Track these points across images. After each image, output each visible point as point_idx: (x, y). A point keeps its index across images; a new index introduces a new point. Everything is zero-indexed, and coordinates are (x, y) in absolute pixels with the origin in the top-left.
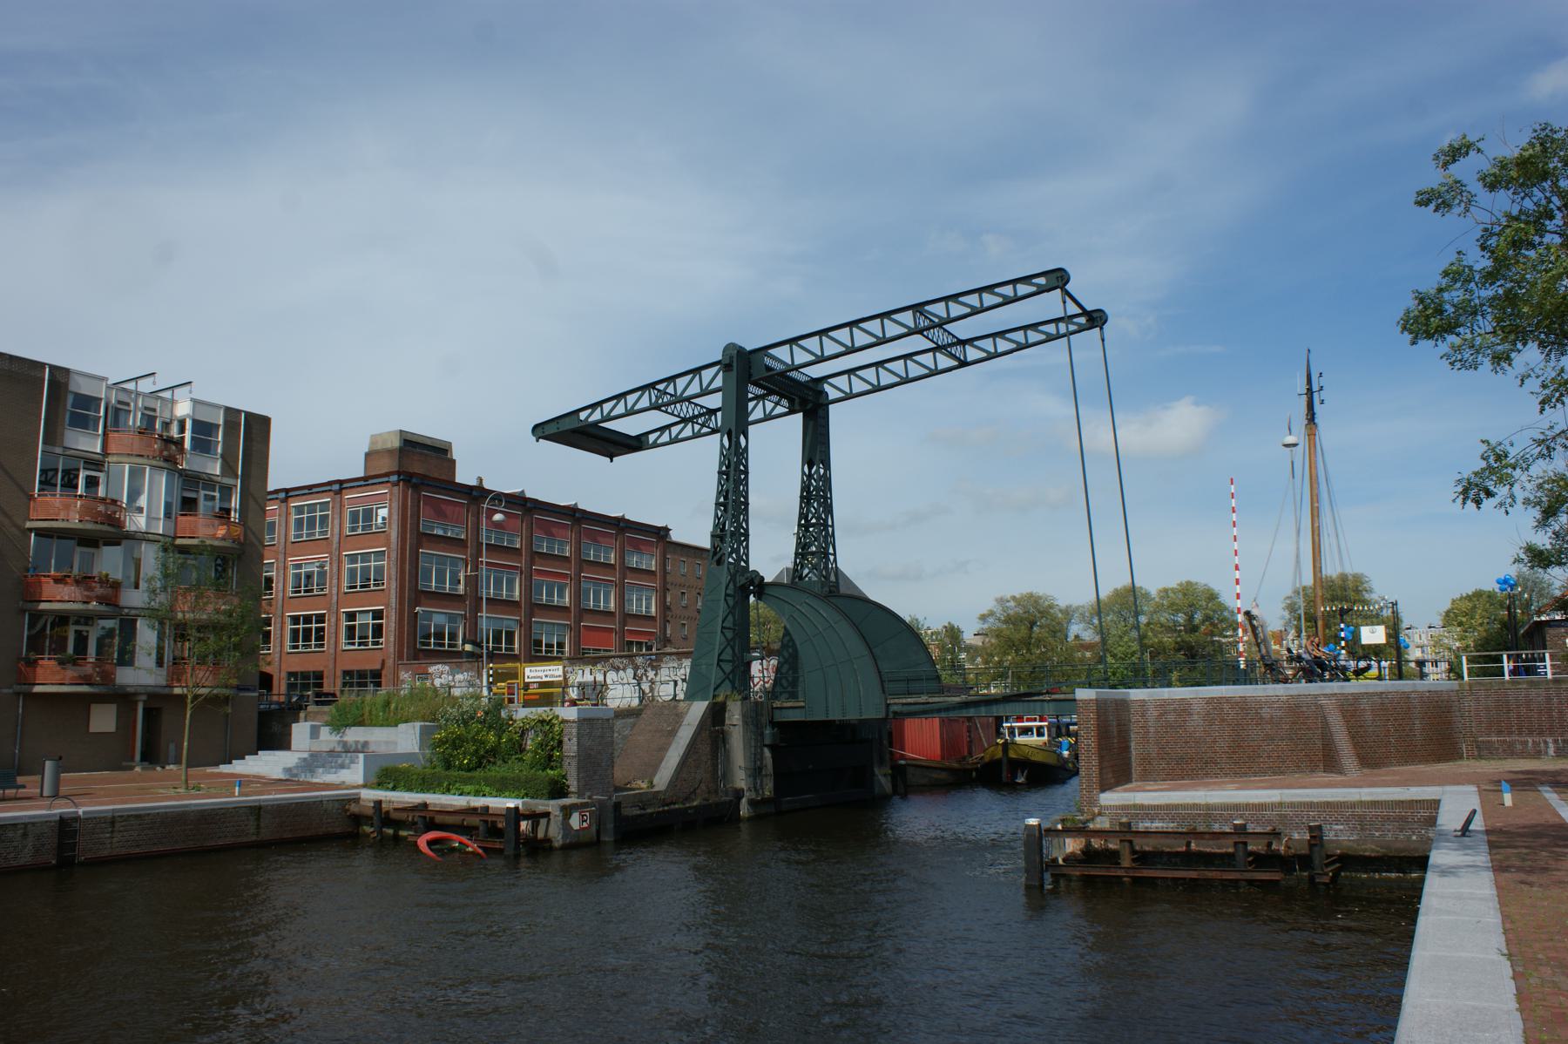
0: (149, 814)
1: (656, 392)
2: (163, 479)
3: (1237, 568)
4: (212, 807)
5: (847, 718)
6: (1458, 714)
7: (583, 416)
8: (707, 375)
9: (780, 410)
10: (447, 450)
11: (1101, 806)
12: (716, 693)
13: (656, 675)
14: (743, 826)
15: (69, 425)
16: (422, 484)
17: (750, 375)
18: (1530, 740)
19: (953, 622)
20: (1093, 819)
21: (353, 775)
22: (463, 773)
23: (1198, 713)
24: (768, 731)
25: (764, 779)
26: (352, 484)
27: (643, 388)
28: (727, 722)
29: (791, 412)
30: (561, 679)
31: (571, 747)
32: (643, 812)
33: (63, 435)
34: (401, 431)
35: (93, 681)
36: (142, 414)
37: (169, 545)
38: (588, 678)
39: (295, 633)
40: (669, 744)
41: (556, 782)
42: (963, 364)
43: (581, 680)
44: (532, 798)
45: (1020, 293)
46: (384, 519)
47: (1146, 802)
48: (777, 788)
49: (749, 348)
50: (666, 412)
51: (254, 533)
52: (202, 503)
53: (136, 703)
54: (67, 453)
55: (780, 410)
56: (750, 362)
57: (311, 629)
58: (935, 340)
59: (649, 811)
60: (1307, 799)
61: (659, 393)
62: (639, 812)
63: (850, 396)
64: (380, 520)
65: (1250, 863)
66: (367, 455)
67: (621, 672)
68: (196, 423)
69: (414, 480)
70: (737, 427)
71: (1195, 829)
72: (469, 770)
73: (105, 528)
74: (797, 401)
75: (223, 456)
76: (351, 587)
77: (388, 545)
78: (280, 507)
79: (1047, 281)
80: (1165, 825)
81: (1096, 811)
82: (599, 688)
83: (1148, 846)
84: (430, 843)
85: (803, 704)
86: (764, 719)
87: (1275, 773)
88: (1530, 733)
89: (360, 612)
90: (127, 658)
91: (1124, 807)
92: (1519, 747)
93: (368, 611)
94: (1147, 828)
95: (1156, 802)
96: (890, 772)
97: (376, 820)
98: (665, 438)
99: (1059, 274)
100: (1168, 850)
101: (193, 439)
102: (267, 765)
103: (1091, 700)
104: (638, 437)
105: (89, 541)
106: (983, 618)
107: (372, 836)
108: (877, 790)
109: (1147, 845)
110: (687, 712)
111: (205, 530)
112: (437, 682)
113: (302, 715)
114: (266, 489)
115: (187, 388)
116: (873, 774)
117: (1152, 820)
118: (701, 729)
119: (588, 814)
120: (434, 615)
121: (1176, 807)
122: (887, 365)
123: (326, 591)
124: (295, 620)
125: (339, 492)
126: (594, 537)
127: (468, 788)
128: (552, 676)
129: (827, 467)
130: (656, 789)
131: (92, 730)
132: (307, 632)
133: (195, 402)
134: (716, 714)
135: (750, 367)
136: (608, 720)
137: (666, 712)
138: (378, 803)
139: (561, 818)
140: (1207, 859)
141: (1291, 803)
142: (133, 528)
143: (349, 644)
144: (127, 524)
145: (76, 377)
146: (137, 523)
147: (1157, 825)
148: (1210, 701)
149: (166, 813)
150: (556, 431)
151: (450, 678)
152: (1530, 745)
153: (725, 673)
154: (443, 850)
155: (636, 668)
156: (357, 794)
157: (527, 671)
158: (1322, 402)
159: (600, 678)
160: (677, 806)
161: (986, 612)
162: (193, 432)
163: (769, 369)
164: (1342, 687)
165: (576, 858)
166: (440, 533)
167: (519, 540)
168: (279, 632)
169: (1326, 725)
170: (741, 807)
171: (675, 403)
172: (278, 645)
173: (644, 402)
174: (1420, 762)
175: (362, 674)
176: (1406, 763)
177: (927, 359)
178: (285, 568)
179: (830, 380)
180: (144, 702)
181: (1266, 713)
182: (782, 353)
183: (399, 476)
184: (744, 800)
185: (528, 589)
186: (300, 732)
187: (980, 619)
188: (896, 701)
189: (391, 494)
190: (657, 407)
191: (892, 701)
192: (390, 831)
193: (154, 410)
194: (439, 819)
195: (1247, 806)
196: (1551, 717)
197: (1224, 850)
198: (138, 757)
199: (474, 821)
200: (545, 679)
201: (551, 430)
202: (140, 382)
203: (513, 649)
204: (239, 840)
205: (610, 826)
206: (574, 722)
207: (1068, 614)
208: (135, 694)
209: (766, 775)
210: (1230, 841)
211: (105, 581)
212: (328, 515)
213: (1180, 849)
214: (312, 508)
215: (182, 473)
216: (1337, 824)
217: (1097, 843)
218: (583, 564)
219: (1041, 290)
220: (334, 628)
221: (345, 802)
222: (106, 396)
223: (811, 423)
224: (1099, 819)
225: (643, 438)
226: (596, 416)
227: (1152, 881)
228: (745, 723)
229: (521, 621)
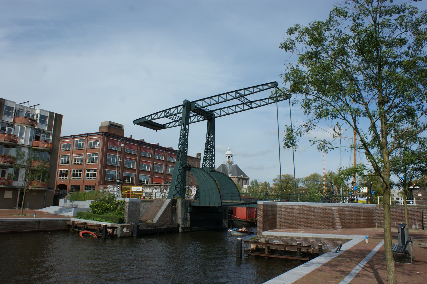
0: (5, 221)
1: (166, 112)
2: (30, 130)
3: (324, 169)
4: (25, 220)
5: (215, 206)
6: (375, 214)
7: (147, 118)
8: (180, 108)
9: (201, 119)
10: (122, 127)
11: (262, 235)
12: (174, 197)
13: (166, 191)
14: (180, 234)
15: (4, 114)
16: (109, 135)
17: (191, 109)
18: (396, 223)
19: (266, 181)
20: (260, 239)
21: (70, 214)
22: (98, 215)
23: (296, 210)
24: (189, 208)
25: (187, 222)
26: (91, 135)
27: (162, 111)
28: (177, 205)
29: (204, 120)
30: (141, 191)
31: (127, 209)
32: (147, 229)
33: (2, 117)
34: (109, 121)
35: (5, 184)
36: (26, 112)
37: (30, 148)
38: (148, 191)
39: (74, 174)
40: (159, 210)
41: (121, 219)
42: (251, 108)
43: (146, 191)
44: (114, 223)
45: (264, 88)
46: (98, 144)
47: (275, 235)
48: (191, 224)
49: (191, 101)
50: (169, 118)
51: (56, 146)
52: (41, 137)
53: (18, 191)
54: (3, 122)
55: (201, 119)
56: (191, 105)
57: (78, 174)
58: (242, 101)
59: (149, 228)
60: (320, 237)
61: (167, 113)
62: (145, 229)
63: (220, 116)
64: (97, 145)
65: (301, 255)
66: (100, 127)
67: (157, 190)
68: (41, 116)
69: (107, 134)
70: (186, 122)
71: (288, 244)
72: (100, 214)
73: (12, 143)
74: (206, 116)
75: (48, 125)
76: (89, 163)
77: (99, 152)
78: (72, 140)
79: (272, 85)
80: (280, 242)
81: (261, 237)
82: (151, 194)
83: (274, 248)
84: (83, 234)
85: (199, 201)
86: (188, 205)
87: (318, 229)
88: (396, 221)
89: (91, 170)
90: (16, 179)
91: (269, 236)
92: (392, 225)
93: (93, 170)
94: (275, 243)
95: (278, 235)
96: (228, 222)
97: (72, 226)
98: (171, 125)
99: (275, 83)
100: (279, 249)
101: (40, 120)
102: (51, 210)
103: (262, 204)
104: (164, 125)
105: (8, 146)
106: (274, 180)
107: (71, 231)
108: (223, 226)
109: (273, 248)
110: (165, 202)
111: (41, 145)
112: (109, 190)
113: (66, 197)
114: (60, 135)
115: (38, 106)
116: (222, 222)
117: (276, 240)
118: (168, 206)
119: (129, 228)
120: (111, 171)
121: (283, 237)
122: (231, 108)
123: (82, 164)
124: (74, 171)
125: (87, 137)
126: (158, 153)
127: (98, 219)
128: (139, 190)
129: (214, 135)
130: (153, 222)
131: (5, 197)
132: (77, 174)
133: (41, 110)
134: (174, 202)
135: (191, 107)
136: (139, 202)
137: (160, 201)
138: (74, 222)
139: (120, 229)
140: (291, 253)
141: (316, 238)
142: (20, 143)
143: (87, 178)
144: (19, 142)
145: (7, 102)
146: (22, 142)
147: (277, 242)
148: (300, 206)
149: (11, 221)
150: (139, 122)
151: (113, 189)
152: (396, 224)
153: (177, 191)
154: (86, 236)
155: (161, 189)
156: (70, 219)
157: (133, 188)
158: (358, 123)
159: (151, 191)
160: (158, 228)
161: (275, 179)
162: (40, 118)
163: (196, 107)
164: (316, 204)
165: (125, 241)
166: (114, 149)
167: (137, 152)
168: (69, 174)
169: (333, 215)
170: (179, 229)
171: (172, 116)
172: (69, 177)
173: (163, 115)
174: (362, 228)
175: (90, 187)
176: (358, 228)
177: (241, 106)
178: (72, 157)
179: (215, 111)
180: (20, 191)
181: (316, 211)
182: (200, 103)
183: (103, 133)
184: (180, 227)
185: (138, 166)
186: (61, 201)
187: (273, 181)
188: (224, 202)
189: (101, 138)
190: (166, 117)
191: (223, 202)
192: (77, 230)
193: (30, 112)
194: (89, 227)
195: (303, 238)
196: (402, 216)
197: (295, 251)
198: (17, 206)
199: (97, 228)
200: (137, 191)
201: (138, 122)
202: (25, 104)
203: (133, 182)
204: (33, 230)
205: (136, 232)
206: (128, 202)
207: (298, 180)
208: (18, 188)
209: (188, 221)
210: (296, 248)
211: (11, 157)
212: (84, 143)
213: (282, 249)
214: (80, 141)
215: (36, 129)
216: (328, 245)
217: (259, 246)
218: (155, 160)
219: (270, 88)
220: (84, 174)
221: (65, 221)
222: (15, 107)
223: (210, 123)
224: (262, 239)
225: (165, 125)
226: (150, 119)
227: (272, 258)
228: (182, 206)
229: (136, 174)
